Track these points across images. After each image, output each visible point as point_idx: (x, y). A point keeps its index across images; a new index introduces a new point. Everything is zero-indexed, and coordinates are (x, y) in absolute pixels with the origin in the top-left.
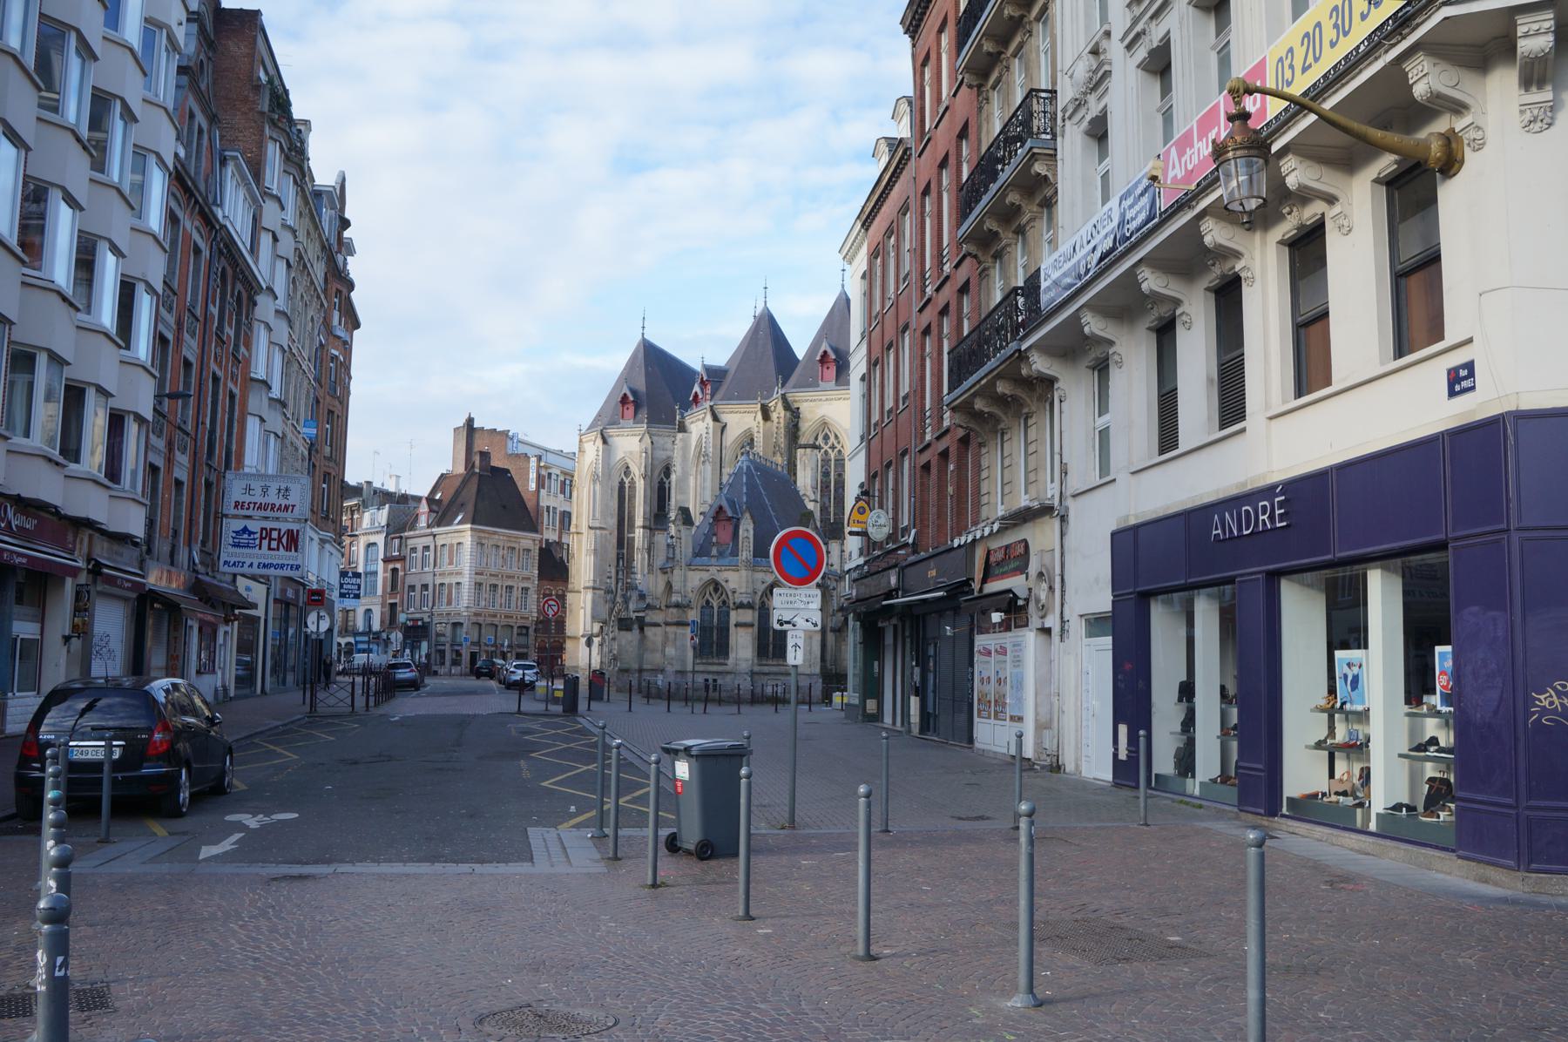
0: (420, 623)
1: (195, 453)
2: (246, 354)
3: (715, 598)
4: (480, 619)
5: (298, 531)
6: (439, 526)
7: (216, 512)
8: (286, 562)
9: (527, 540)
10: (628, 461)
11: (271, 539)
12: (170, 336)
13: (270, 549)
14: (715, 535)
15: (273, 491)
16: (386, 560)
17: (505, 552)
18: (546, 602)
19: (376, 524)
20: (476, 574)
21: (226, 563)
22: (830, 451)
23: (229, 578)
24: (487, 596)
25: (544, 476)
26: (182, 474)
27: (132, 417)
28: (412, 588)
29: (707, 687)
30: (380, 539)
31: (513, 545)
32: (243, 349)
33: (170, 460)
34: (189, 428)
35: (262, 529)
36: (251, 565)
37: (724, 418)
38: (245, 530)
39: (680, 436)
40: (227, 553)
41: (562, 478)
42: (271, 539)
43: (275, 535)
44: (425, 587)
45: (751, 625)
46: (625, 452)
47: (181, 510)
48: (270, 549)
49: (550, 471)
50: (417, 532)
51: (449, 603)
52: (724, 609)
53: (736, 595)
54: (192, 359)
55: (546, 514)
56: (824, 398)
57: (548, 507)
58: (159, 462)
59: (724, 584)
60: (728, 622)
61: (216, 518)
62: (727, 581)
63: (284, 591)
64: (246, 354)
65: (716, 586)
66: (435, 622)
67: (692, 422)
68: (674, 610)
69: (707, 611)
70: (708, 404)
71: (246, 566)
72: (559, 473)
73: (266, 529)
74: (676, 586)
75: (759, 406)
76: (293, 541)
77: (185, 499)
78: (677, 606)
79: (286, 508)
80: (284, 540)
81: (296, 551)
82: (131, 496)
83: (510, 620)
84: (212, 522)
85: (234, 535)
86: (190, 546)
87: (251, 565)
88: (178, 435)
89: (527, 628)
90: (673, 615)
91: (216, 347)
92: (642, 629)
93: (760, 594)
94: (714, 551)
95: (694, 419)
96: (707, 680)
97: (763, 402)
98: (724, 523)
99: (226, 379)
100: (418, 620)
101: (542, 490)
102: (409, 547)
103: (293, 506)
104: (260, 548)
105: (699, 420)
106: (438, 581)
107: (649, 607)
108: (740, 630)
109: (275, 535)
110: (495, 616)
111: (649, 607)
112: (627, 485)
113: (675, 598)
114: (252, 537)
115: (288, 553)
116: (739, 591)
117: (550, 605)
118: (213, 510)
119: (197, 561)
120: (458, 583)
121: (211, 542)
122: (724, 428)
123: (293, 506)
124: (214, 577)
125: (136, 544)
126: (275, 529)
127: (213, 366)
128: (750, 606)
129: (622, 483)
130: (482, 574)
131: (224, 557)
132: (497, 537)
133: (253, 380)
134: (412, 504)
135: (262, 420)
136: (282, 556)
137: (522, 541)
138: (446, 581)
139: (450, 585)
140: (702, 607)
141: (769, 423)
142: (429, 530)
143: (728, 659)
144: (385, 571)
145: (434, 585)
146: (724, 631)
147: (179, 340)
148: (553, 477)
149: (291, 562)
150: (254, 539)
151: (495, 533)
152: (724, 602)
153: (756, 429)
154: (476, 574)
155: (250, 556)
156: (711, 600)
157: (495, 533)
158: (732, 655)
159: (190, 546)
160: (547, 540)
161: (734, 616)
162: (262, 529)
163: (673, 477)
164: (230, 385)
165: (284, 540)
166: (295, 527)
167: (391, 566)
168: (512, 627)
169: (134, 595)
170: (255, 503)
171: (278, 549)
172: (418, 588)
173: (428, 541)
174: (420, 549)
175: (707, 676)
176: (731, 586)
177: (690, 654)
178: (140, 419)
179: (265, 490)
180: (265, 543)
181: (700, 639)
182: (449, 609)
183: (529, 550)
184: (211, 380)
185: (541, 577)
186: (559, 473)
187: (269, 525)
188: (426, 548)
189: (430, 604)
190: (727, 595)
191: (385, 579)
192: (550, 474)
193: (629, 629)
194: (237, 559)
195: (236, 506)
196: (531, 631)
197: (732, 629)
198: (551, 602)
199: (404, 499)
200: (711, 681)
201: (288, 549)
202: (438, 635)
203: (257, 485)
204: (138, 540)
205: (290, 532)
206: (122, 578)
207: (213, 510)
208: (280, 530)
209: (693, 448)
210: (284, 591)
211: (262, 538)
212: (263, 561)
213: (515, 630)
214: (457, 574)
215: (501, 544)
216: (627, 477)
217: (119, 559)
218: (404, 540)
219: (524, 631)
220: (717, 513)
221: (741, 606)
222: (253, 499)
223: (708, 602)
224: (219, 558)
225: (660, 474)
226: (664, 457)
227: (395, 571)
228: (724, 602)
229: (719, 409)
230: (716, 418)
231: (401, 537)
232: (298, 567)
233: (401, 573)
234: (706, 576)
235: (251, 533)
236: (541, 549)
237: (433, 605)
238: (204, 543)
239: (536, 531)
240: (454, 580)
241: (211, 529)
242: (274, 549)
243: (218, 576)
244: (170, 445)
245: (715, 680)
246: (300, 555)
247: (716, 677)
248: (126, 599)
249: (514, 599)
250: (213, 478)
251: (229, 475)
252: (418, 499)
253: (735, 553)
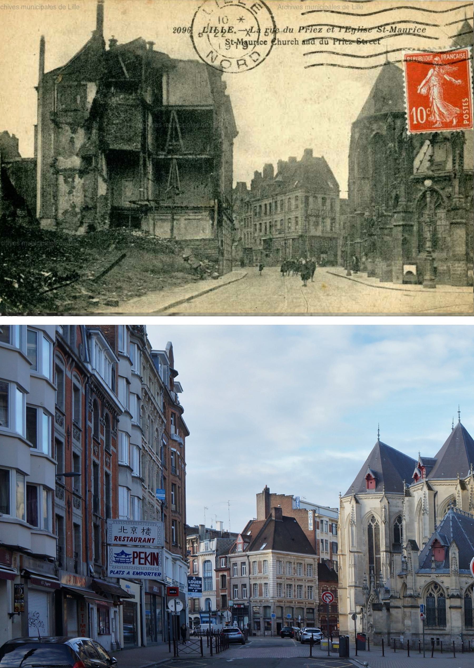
0: (242, 606)
1: (86, 508)
2: (115, 450)
4: (282, 604)
5: (157, 554)
6: (250, 550)
7: (103, 543)
8: (151, 571)
9: (309, 559)
10: (373, 513)
11: (140, 558)
12: (63, 440)
13: (140, 563)
14: (433, 556)
15: (139, 530)
16: (217, 570)
17: (296, 566)
18: (325, 594)
19: (209, 550)
20: (277, 578)
21: (111, 572)
23: (115, 581)
24: (286, 591)
25: (318, 522)
26: (79, 522)
27: (42, 488)
28: (236, 586)
29: (433, 643)
30: (213, 558)
31: (300, 562)
32: (112, 448)
33: (69, 513)
34: (80, 493)
35: (134, 552)
36: (129, 573)
37: (436, 488)
38: (123, 553)
39: (407, 499)
40: (112, 566)
41: (330, 523)
42: (140, 558)
43: (143, 556)
44: (244, 586)
45: (460, 608)
47: (79, 542)
48: (140, 563)
49: (322, 519)
50: (236, 554)
51: (261, 595)
52: (442, 598)
53: (449, 591)
54: (79, 453)
55: (321, 544)
57: (322, 540)
58: (63, 514)
59: (441, 584)
60: (445, 606)
61: (103, 546)
62: (442, 582)
63: (151, 588)
64: (115, 450)
65: (436, 585)
66: (252, 606)
67: (415, 491)
68: (409, 599)
69: (431, 599)
70: (424, 480)
71: (125, 573)
72: (328, 520)
73: (136, 552)
74: (409, 585)
75: (458, 481)
76: (155, 559)
77: (81, 535)
78: (411, 596)
79: (149, 540)
80: (149, 559)
81: (157, 565)
82: (46, 533)
83: (301, 605)
84: (100, 548)
85: (116, 556)
86: (87, 561)
87: (129, 573)
88: (73, 498)
89: (313, 609)
90: (408, 601)
91: (94, 447)
92: (388, 610)
93: (464, 590)
94: (433, 565)
95: (416, 489)
97: (461, 479)
98: (438, 549)
99: (102, 465)
100: (241, 604)
101: (317, 530)
102: (232, 563)
103: (154, 539)
104: (134, 563)
105: (419, 489)
106: (253, 582)
107: (392, 597)
108: (453, 611)
109: (143, 556)
110: (291, 602)
111: (392, 597)
112: (373, 527)
113: (409, 592)
114: (128, 557)
115: (152, 566)
116: (450, 588)
117: (327, 596)
118: (100, 542)
119: (92, 571)
120: (266, 584)
121: (101, 560)
122: (436, 494)
123: (154, 539)
124: (105, 580)
125: (51, 561)
126: (143, 553)
127: (93, 458)
128: (458, 597)
129: (370, 526)
130: (281, 578)
131: (110, 569)
132: (289, 557)
133: (120, 465)
134: (232, 538)
135: (129, 489)
136: (148, 568)
137: (306, 559)
138: (258, 582)
139: (261, 585)
140: (427, 597)
141: (465, 491)
142: (244, 553)
143: (446, 626)
144: (217, 576)
145: (250, 585)
146: (442, 611)
147: (69, 442)
148: (324, 522)
149: (155, 571)
150: (129, 558)
151: (288, 555)
152: (441, 595)
153: (457, 495)
154: (277, 578)
155: (128, 568)
156: (432, 593)
157: (288, 555)
158: (448, 625)
159: (87, 561)
160: (323, 559)
161: (448, 603)
162: (134, 552)
163: (404, 523)
164: (105, 469)
165: (149, 559)
166: (156, 551)
167: (221, 574)
168: (303, 609)
169: (53, 590)
170: (128, 538)
171: (146, 564)
172: (240, 586)
173: (245, 559)
174: (239, 564)
175: (432, 637)
176: (445, 585)
177: (421, 624)
178: (47, 488)
179: (134, 530)
180: (137, 560)
181: (427, 616)
182: (261, 598)
183: (311, 565)
184: (92, 466)
185: (319, 580)
186: (328, 520)
187: (138, 550)
188: (243, 563)
189: (248, 595)
190: (443, 590)
191: (217, 581)
192: (322, 521)
193: (380, 610)
194: (119, 570)
195: (116, 539)
196: (316, 611)
197: (448, 610)
198: (327, 595)
199: (227, 535)
200: (435, 639)
201: (152, 564)
202: (255, 613)
203: (128, 528)
204: (53, 559)
205: (152, 554)
206: (44, 581)
207: (100, 542)
208: (146, 553)
209: (416, 506)
210: (151, 588)
211: (134, 558)
212: (136, 571)
213: (305, 610)
214: (264, 578)
215: (292, 561)
216: (373, 523)
217: (41, 569)
218: (228, 559)
219: (311, 611)
220: (434, 543)
221: (453, 597)
222: (126, 535)
224: (107, 569)
225: (395, 521)
226: (397, 511)
227: (223, 576)
228: (441, 595)
229: (432, 483)
230: (430, 488)
231: (226, 557)
232: (159, 574)
233: (228, 578)
234: (429, 580)
235: (126, 555)
236: (319, 564)
237: (250, 596)
238: (96, 560)
239: (315, 554)
240: (263, 582)
241: (100, 552)
242: (143, 564)
243: (107, 579)
244: (69, 504)
245: (438, 639)
246: (160, 568)
247: (438, 637)
248: (47, 593)
249: (303, 592)
250: (99, 523)
251: (109, 521)
252: (236, 535)
253: (447, 566)
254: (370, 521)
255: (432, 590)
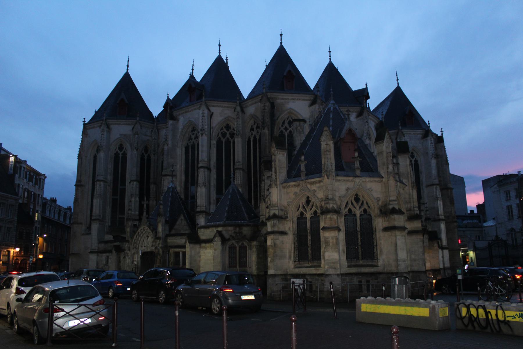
3: (358, 207)
22: (284, 131)
37: (211, 108)
46: (120, 135)
56: (290, 98)
96: (360, 282)
112: (120, 156)
129: (117, 155)
156: (353, 209)
192: (21, 167)
223: (302, 214)
254: (117, 149)
255: (352, 204)
